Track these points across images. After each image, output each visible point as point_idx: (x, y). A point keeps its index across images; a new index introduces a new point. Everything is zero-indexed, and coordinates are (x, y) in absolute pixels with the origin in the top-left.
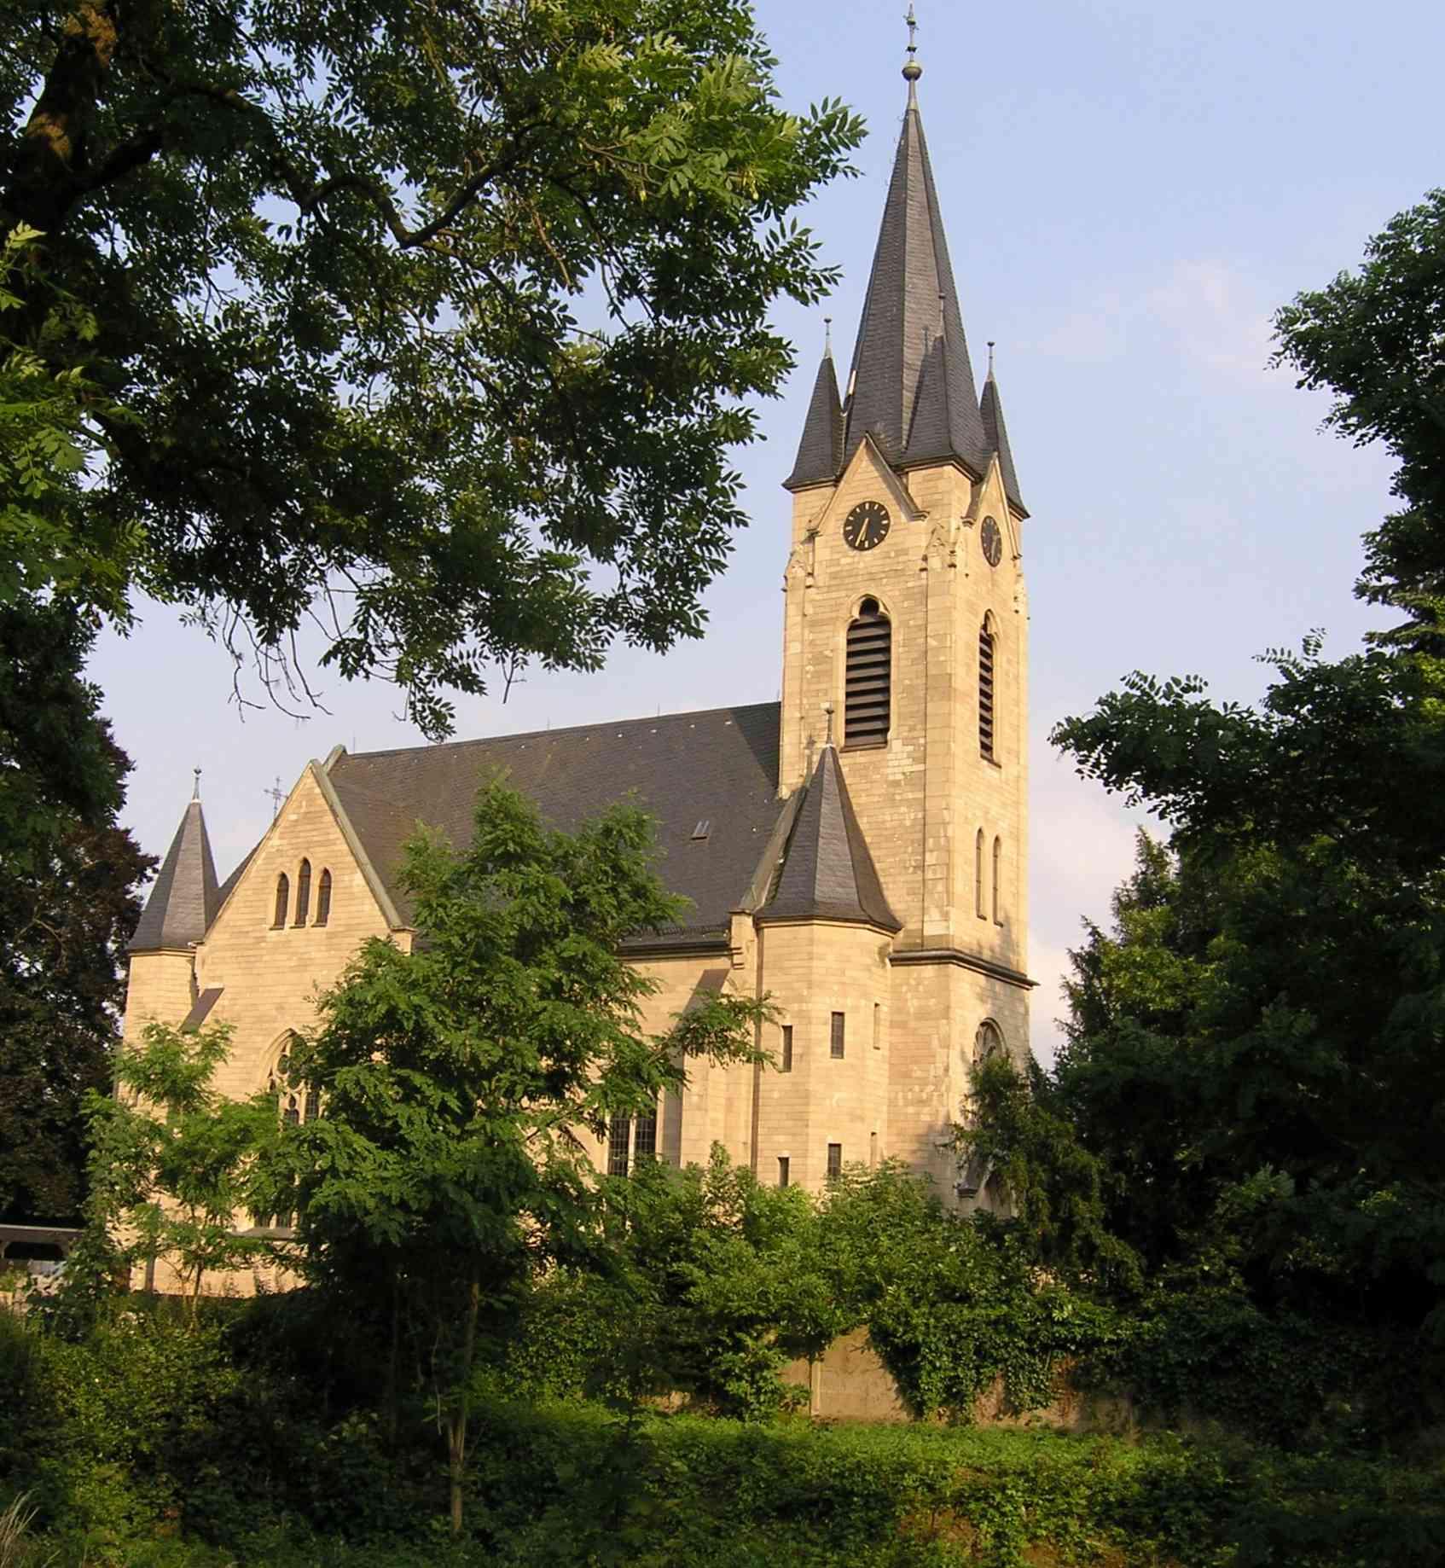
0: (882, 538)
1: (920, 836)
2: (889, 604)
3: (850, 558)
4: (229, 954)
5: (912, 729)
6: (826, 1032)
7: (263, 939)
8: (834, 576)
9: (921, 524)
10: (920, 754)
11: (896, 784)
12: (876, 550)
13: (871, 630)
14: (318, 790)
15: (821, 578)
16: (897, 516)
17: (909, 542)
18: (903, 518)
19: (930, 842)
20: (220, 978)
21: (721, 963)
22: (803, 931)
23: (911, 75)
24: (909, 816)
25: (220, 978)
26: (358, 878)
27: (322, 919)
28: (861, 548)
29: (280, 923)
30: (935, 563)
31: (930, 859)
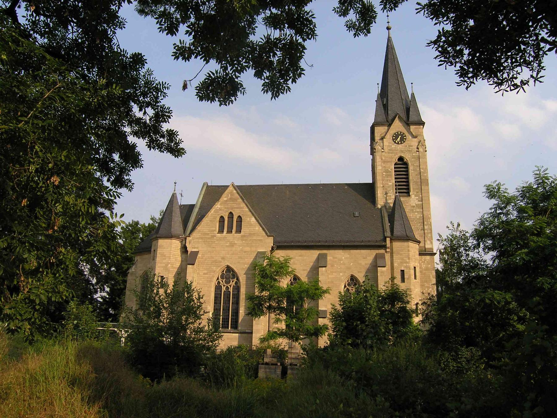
0: (404, 142)
1: (422, 221)
2: (407, 157)
3: (394, 146)
4: (201, 240)
5: (417, 192)
6: (412, 272)
7: (215, 236)
8: (389, 150)
9: (416, 139)
10: (420, 199)
11: (414, 207)
12: (403, 145)
13: (402, 165)
14: (235, 191)
15: (386, 150)
16: (409, 137)
17: (412, 144)
18: (410, 137)
19: (425, 223)
20: (197, 248)
21: (382, 251)
22: (406, 244)
23: (388, 29)
24: (419, 216)
25: (197, 248)
26: (253, 219)
27: (239, 230)
28: (398, 143)
29: (221, 231)
30: (421, 150)
31: (426, 227)
